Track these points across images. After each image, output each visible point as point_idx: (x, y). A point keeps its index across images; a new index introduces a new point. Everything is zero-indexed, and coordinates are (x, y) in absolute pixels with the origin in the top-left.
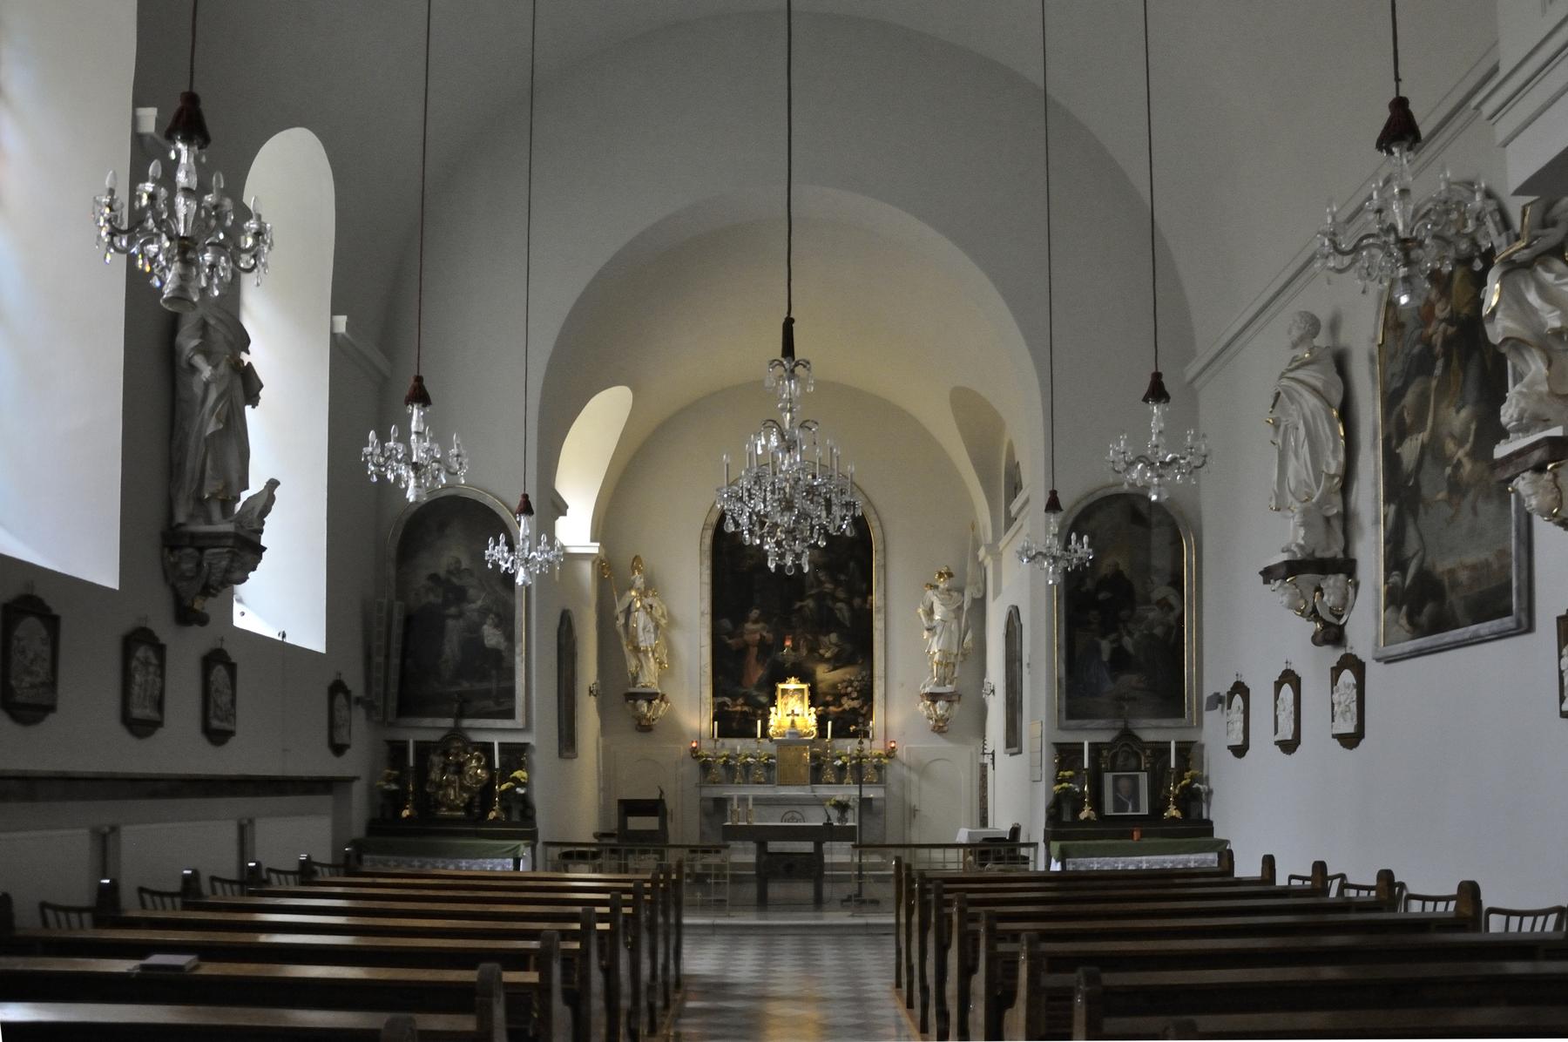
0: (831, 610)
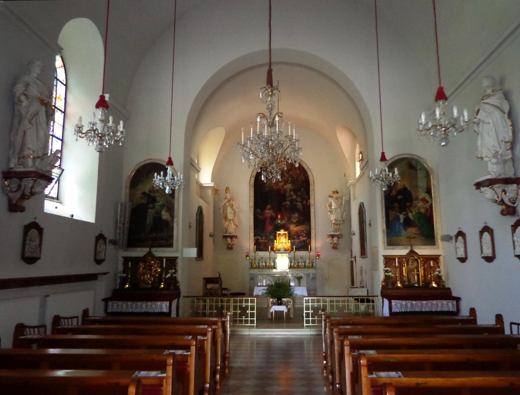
0: (296, 206)
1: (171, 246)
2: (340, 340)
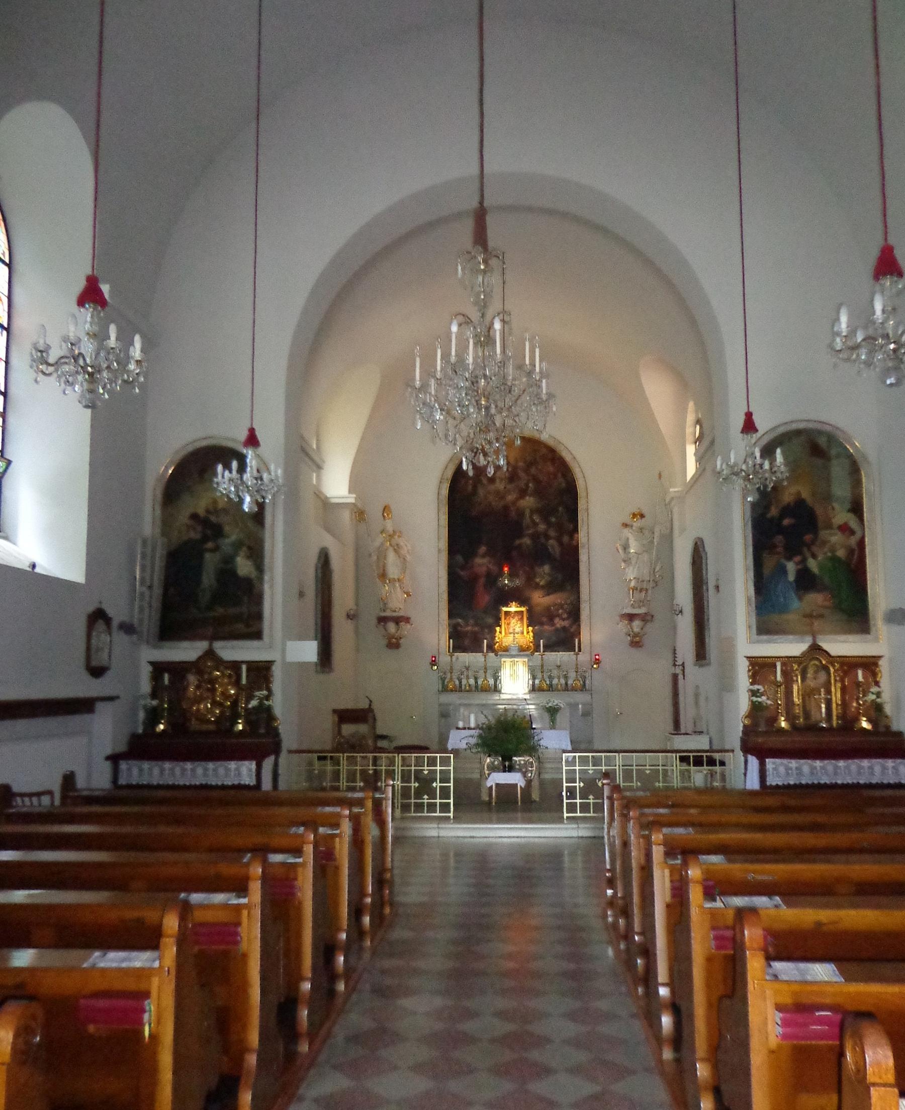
1: (257, 635)
2: (643, 837)
